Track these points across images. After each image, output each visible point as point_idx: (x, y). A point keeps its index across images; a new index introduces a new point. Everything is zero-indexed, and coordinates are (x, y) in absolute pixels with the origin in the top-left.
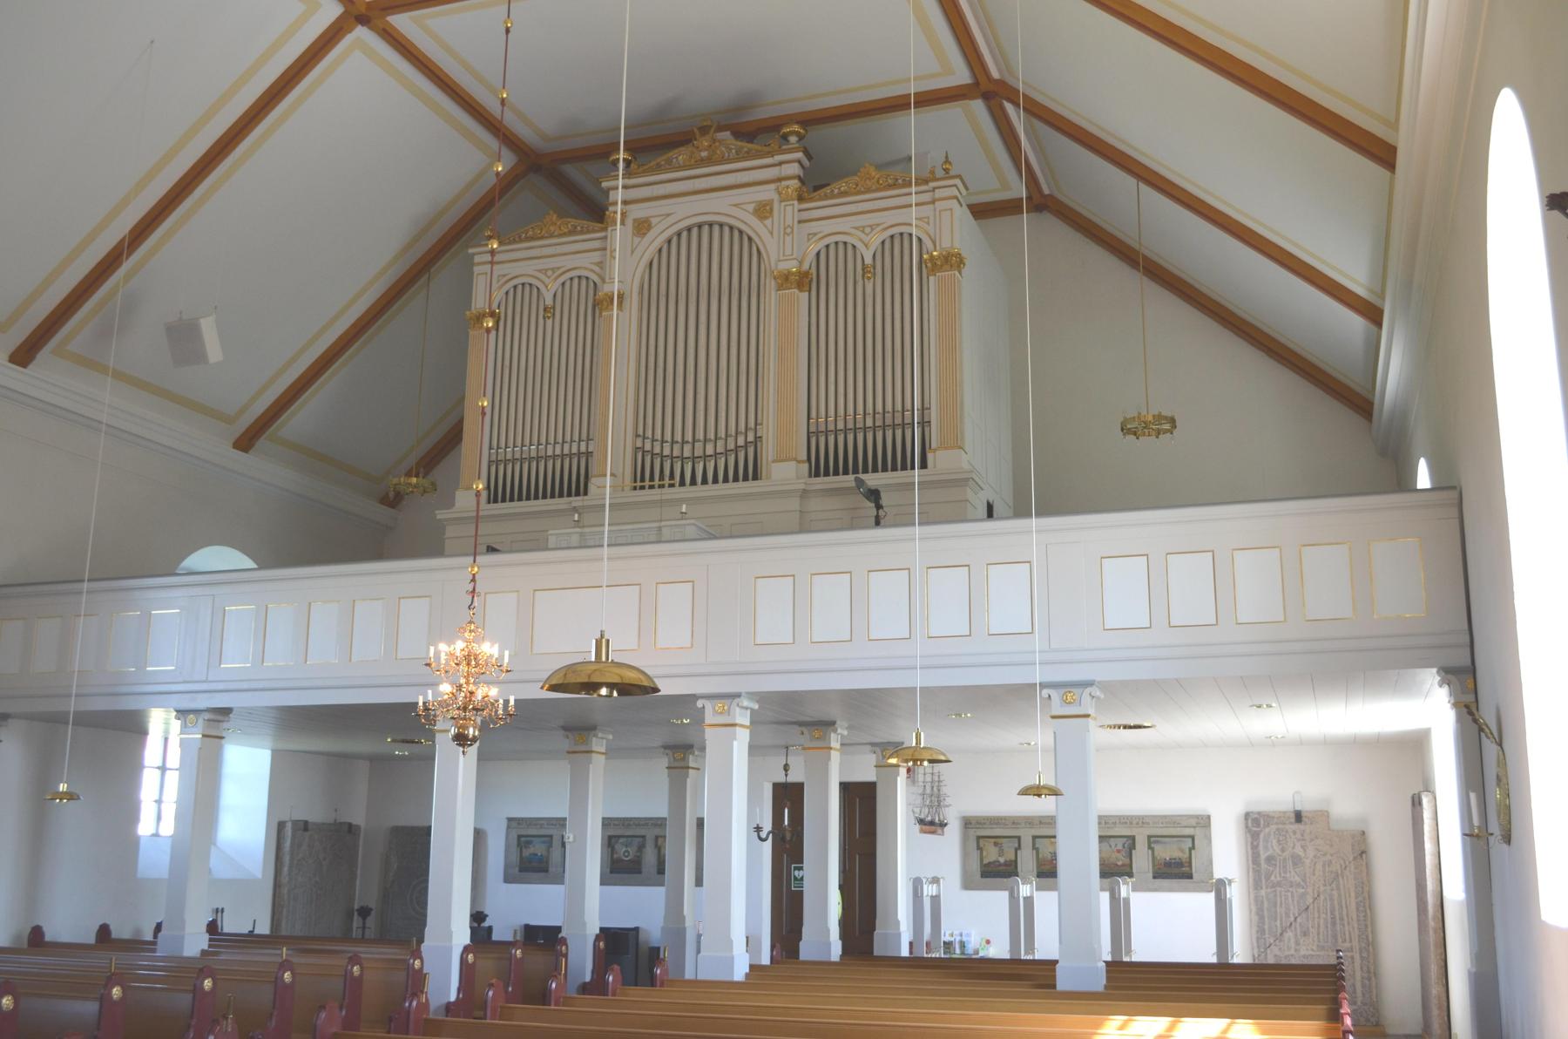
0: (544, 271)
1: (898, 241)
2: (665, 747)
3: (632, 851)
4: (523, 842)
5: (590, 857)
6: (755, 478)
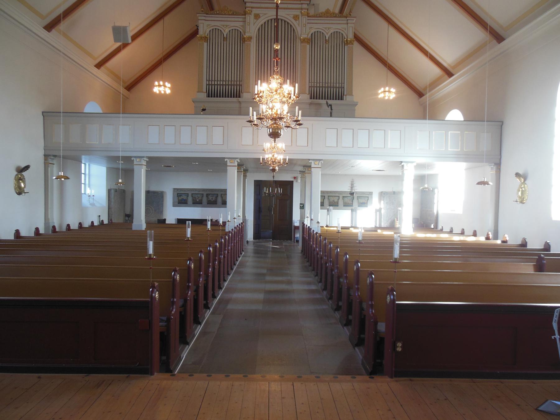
0: (326, 28)
1: (336, 34)
2: (300, 171)
3: (214, 198)
4: (179, 195)
5: (169, 199)
6: (341, 99)
